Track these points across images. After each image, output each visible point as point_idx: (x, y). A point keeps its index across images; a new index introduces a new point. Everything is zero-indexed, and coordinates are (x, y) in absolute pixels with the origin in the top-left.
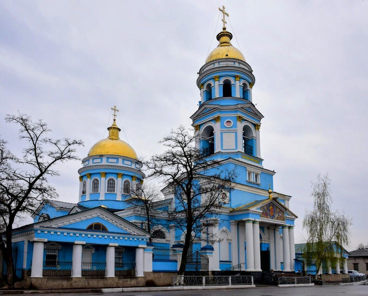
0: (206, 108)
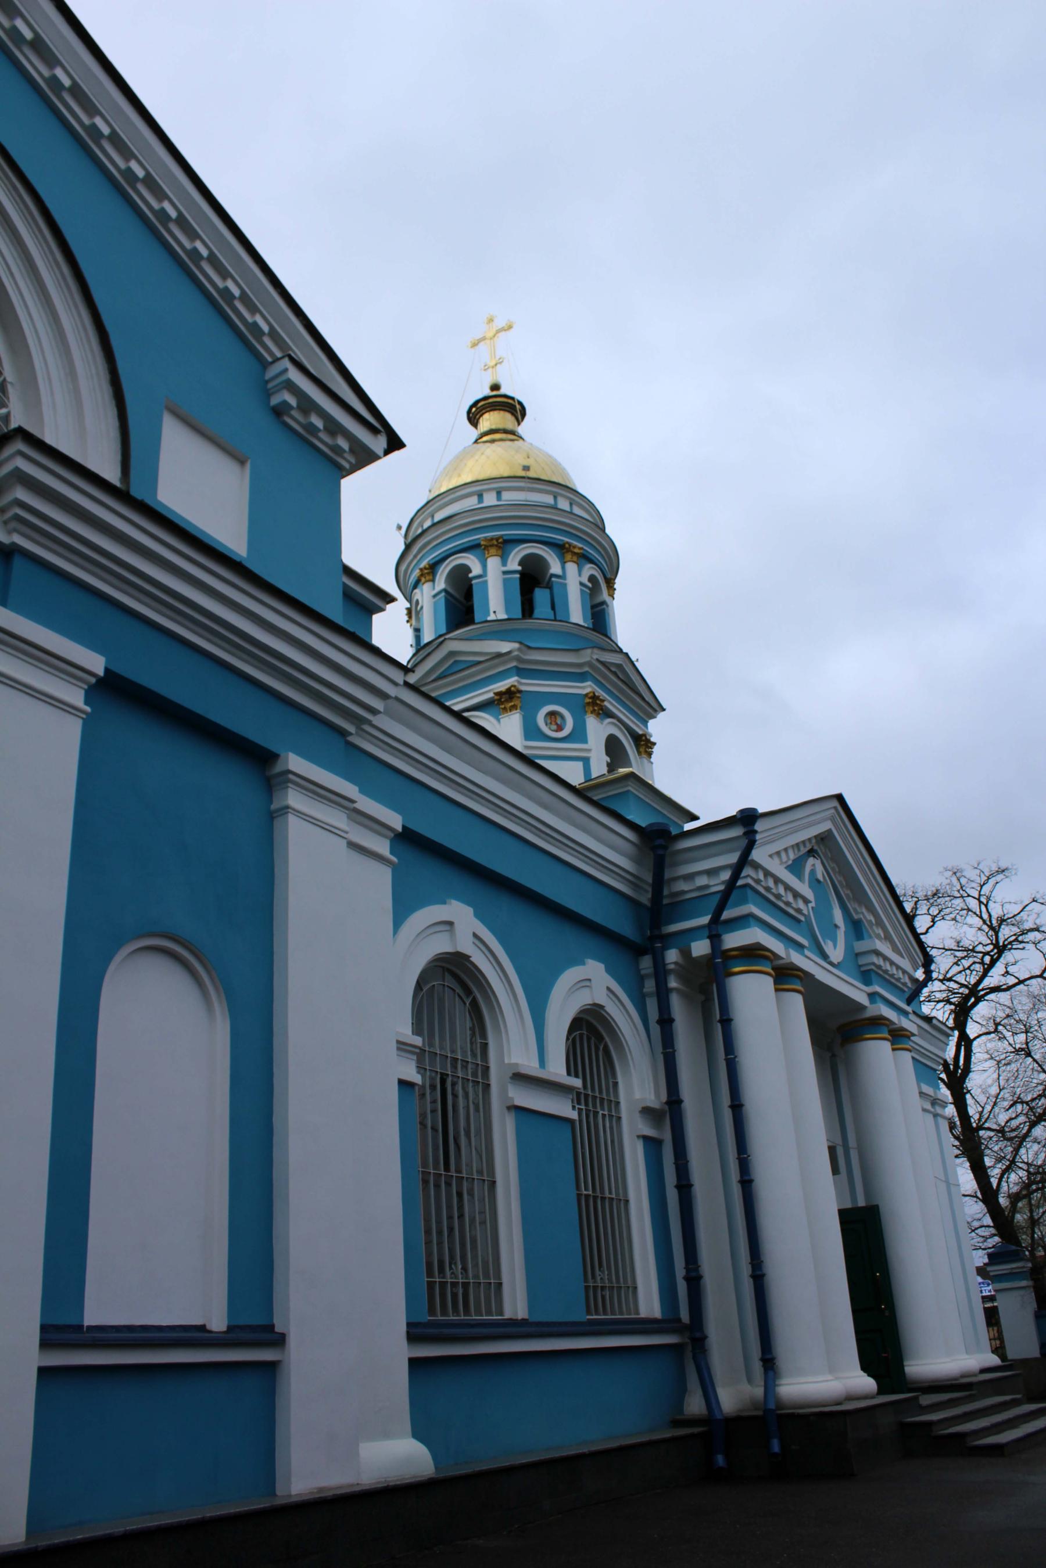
0: (456, 662)
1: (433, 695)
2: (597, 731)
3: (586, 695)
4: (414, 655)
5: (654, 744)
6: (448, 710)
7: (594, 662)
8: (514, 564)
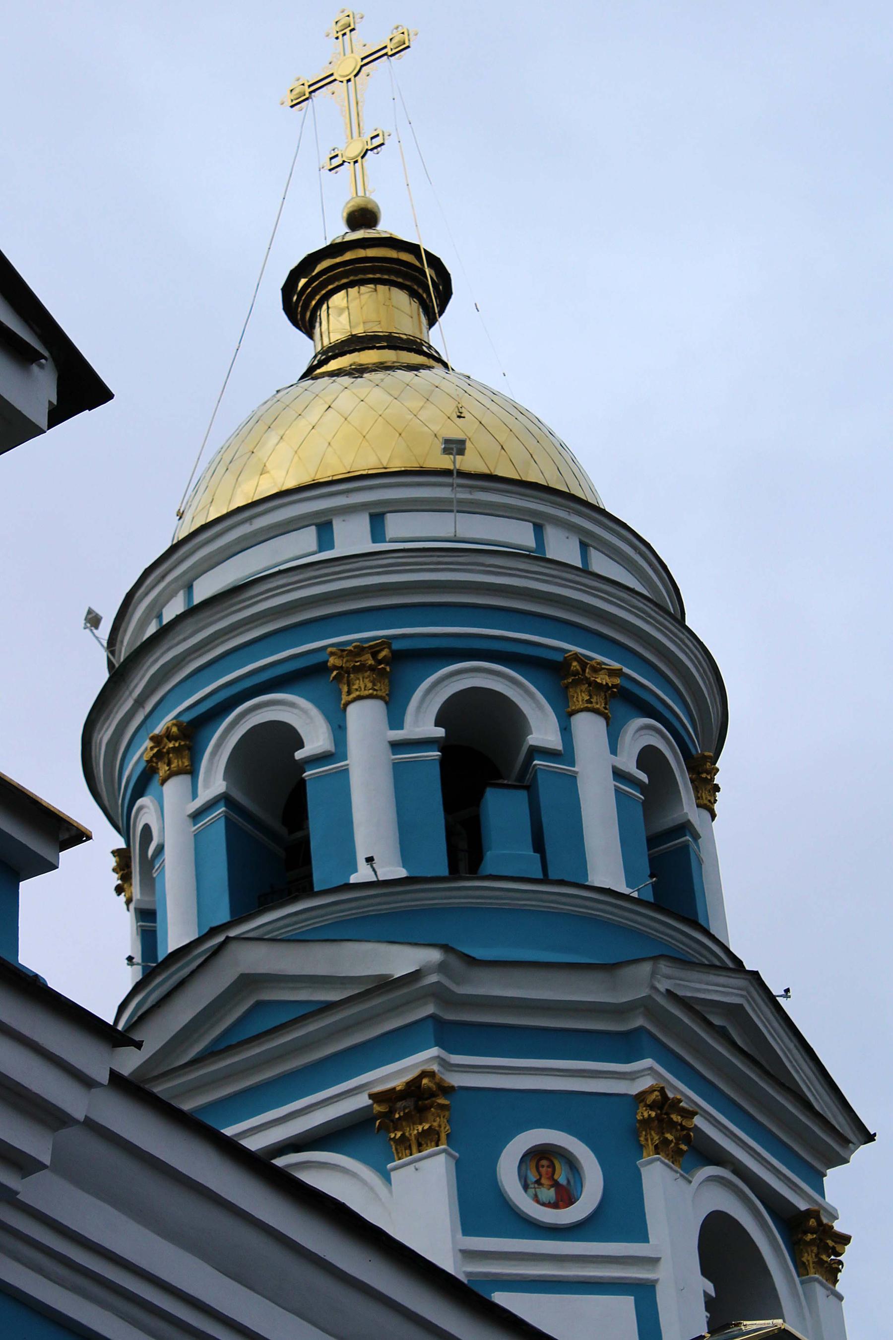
1: (187, 1106)
2: (675, 1204)
3: (641, 1097)
4: (137, 988)
5: (845, 1239)
6: (231, 1150)
7: (662, 1001)
8: (422, 722)
